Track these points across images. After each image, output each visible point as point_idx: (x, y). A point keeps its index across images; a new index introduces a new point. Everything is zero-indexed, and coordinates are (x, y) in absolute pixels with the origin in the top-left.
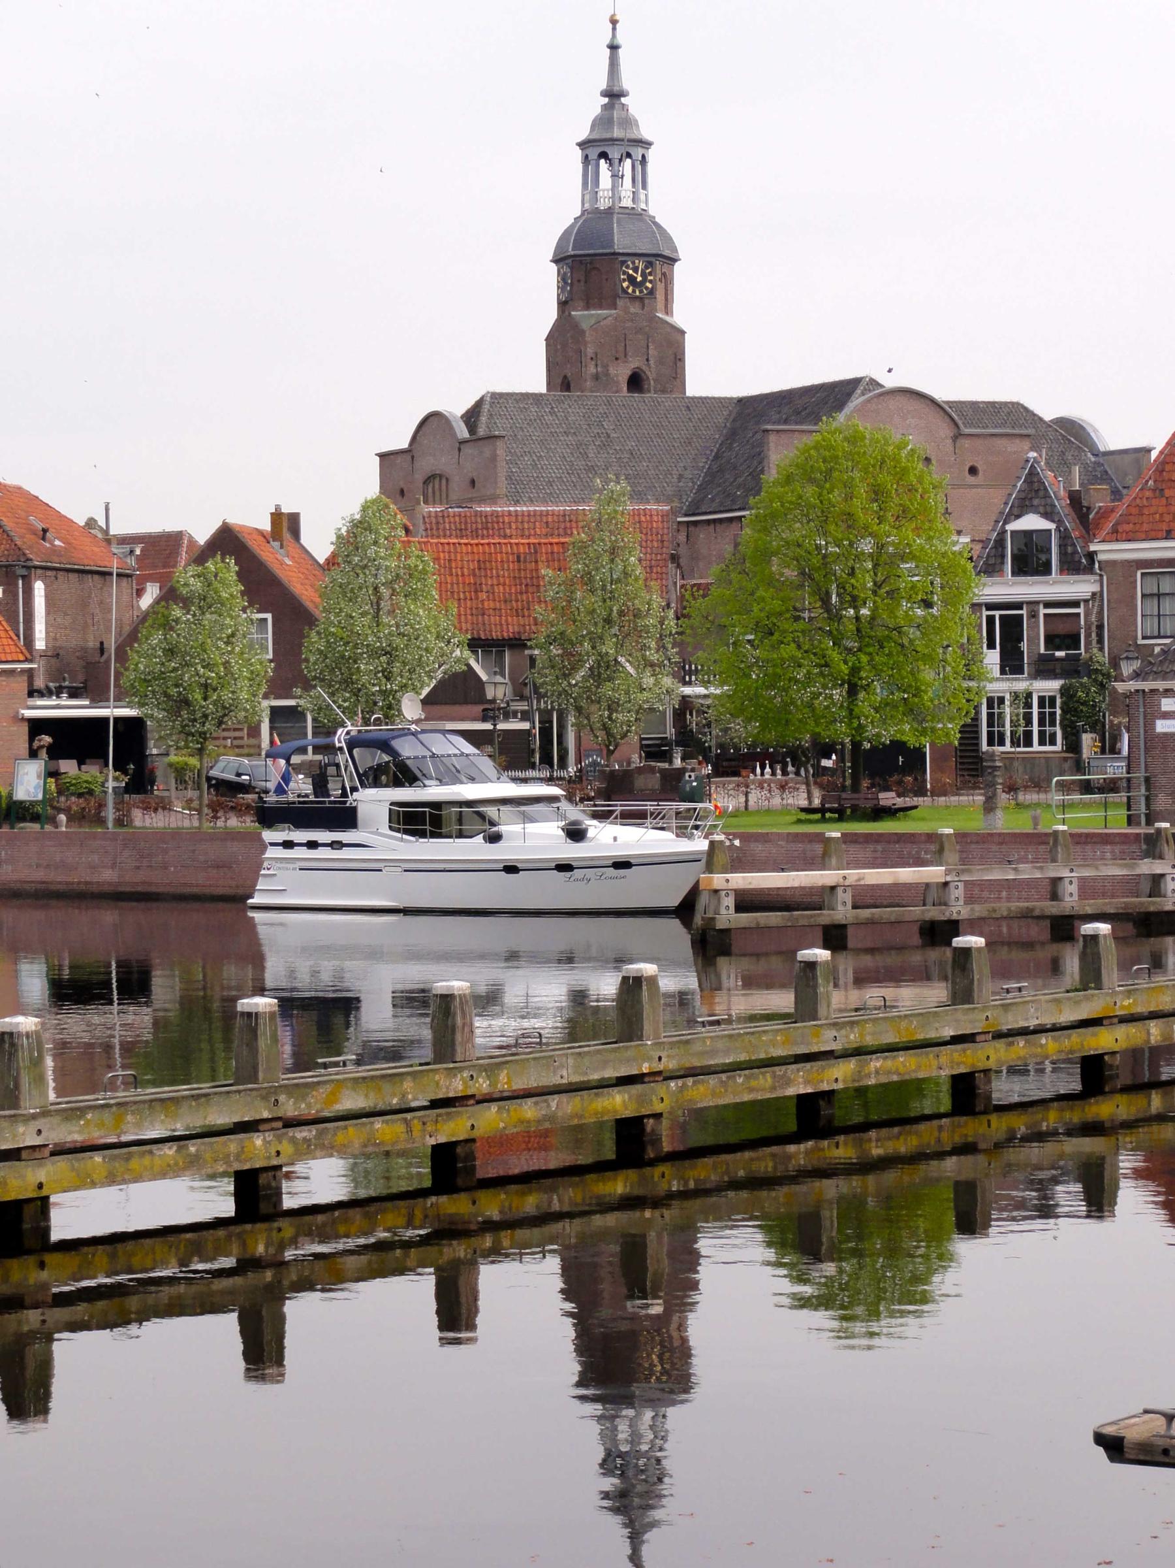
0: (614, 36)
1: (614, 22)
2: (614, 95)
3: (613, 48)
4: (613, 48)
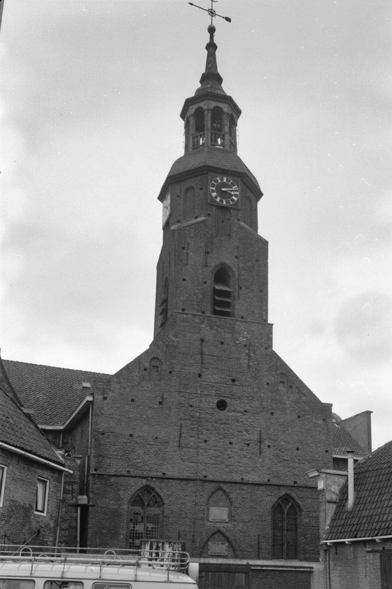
0: (212, 37)
2: (211, 77)
3: (211, 47)
4: (211, 47)
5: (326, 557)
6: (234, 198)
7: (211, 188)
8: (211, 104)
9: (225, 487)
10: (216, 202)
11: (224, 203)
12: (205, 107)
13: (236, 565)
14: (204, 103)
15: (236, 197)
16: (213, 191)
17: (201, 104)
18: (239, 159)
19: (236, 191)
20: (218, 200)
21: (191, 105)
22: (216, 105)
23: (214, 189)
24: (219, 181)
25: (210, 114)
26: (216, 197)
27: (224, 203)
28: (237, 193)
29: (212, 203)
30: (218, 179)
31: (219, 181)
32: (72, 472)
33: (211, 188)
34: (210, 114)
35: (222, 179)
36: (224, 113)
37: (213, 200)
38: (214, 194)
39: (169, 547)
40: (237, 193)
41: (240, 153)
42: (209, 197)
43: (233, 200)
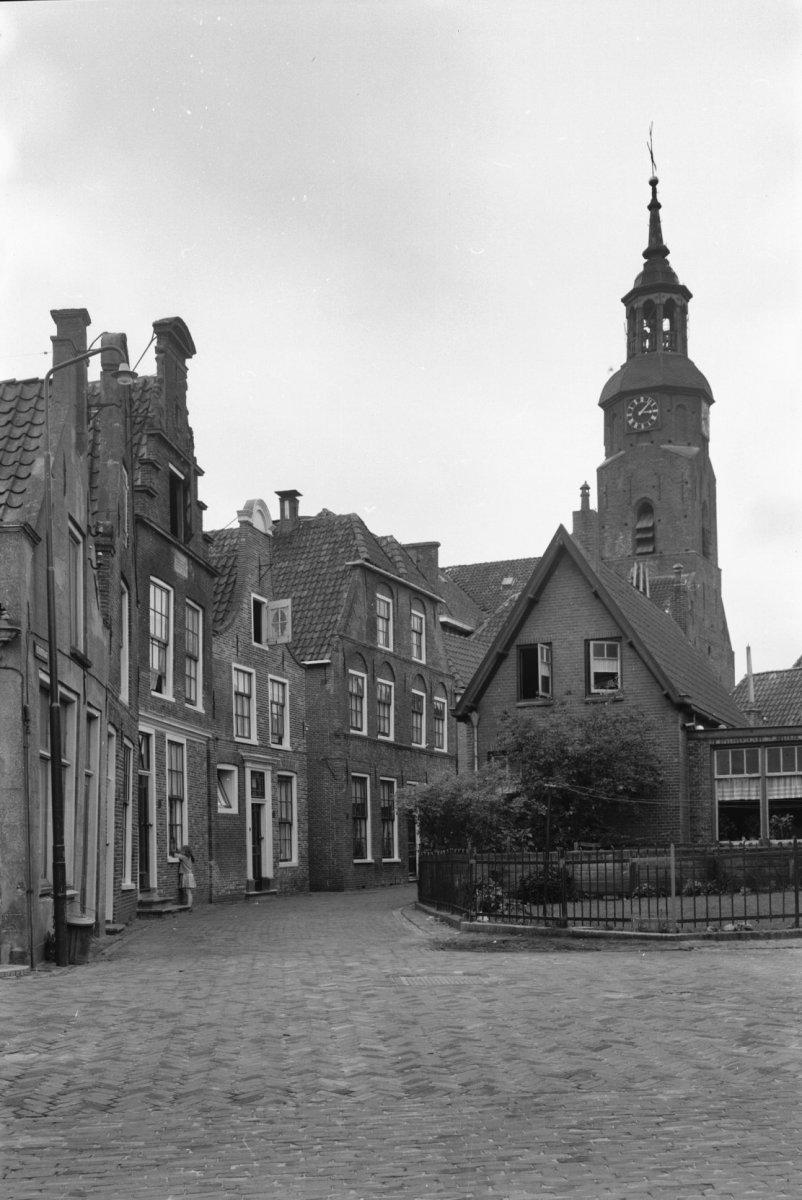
0: (654, 192)
1: (654, 183)
2: (656, 252)
3: (654, 206)
4: (654, 206)
5: (169, 912)
9: (533, 1021)
12: (657, 301)
14: (656, 295)
17: (652, 297)
18: (691, 364)
25: (657, 299)
27: (643, 427)
34: (657, 299)
36: (678, 306)
37: (630, 427)
39: (18, 1044)
41: (693, 354)
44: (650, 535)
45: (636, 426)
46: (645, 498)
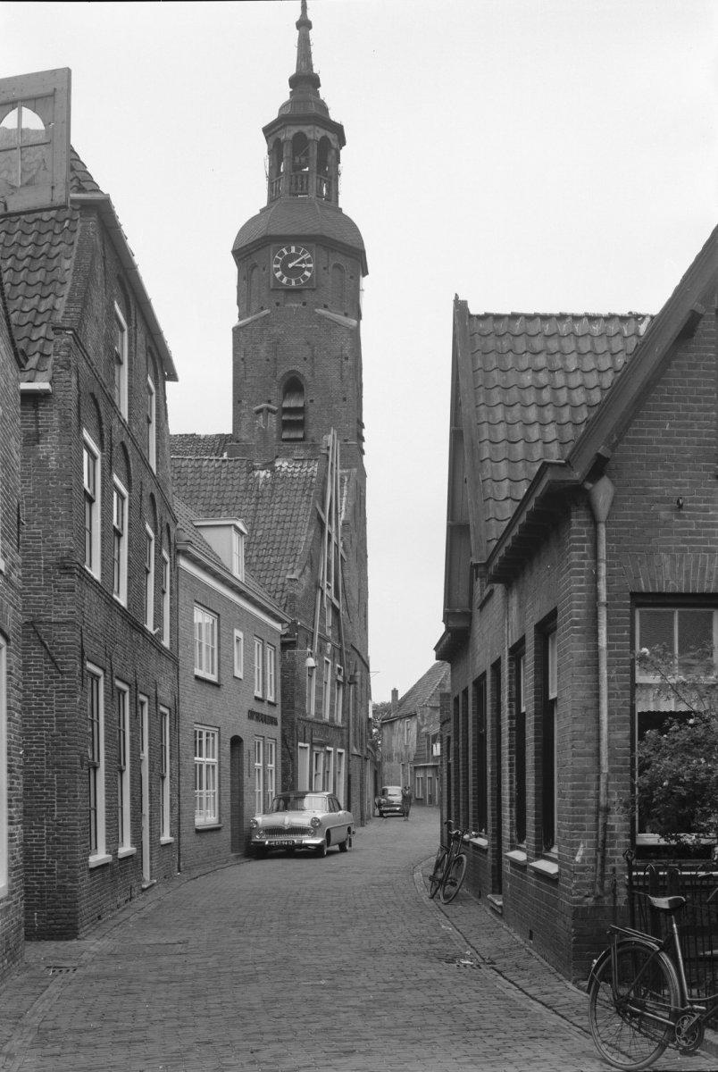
2: (305, 81)
6: (307, 274)
7: (275, 266)
8: (318, 132)
10: (282, 284)
11: (293, 283)
12: (310, 136)
13: (485, 686)
14: (309, 127)
15: (275, 268)
16: (277, 270)
17: (305, 129)
19: (309, 261)
20: (284, 281)
21: (290, 125)
22: (296, 131)
23: (279, 266)
24: (286, 253)
26: (282, 278)
27: (293, 283)
28: (311, 265)
29: (277, 288)
30: (284, 250)
31: (286, 253)
32: (704, 1008)
33: (275, 266)
35: (289, 250)
36: (333, 148)
38: (278, 274)
40: (311, 265)
42: (271, 278)
43: (305, 277)
44: (300, 418)
45: (284, 281)
46: (293, 371)
